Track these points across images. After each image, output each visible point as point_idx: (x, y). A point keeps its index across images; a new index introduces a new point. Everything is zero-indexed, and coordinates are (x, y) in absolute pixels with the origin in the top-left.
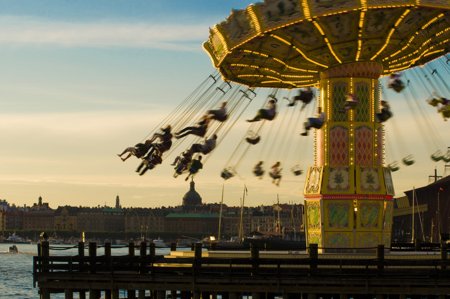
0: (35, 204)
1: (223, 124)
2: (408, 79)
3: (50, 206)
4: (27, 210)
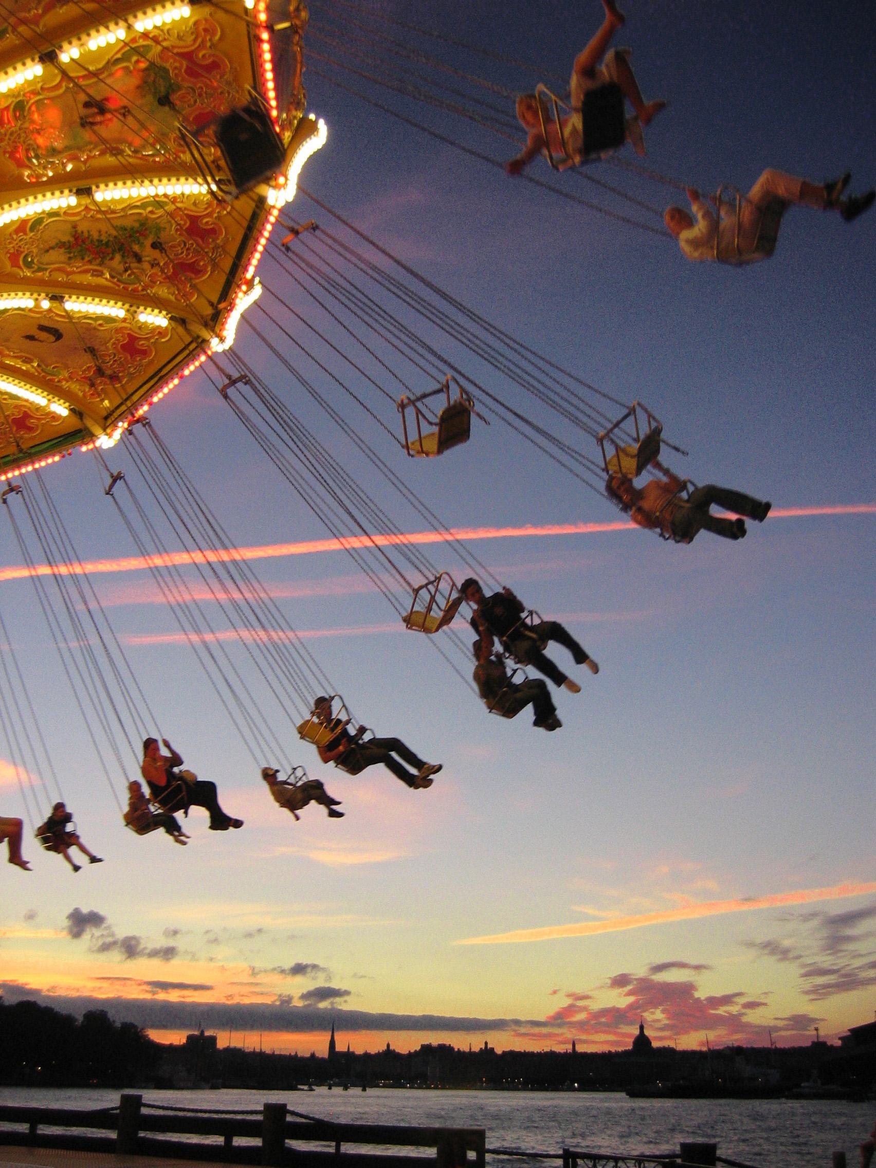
0: (481, 1049)
3: (495, 1050)
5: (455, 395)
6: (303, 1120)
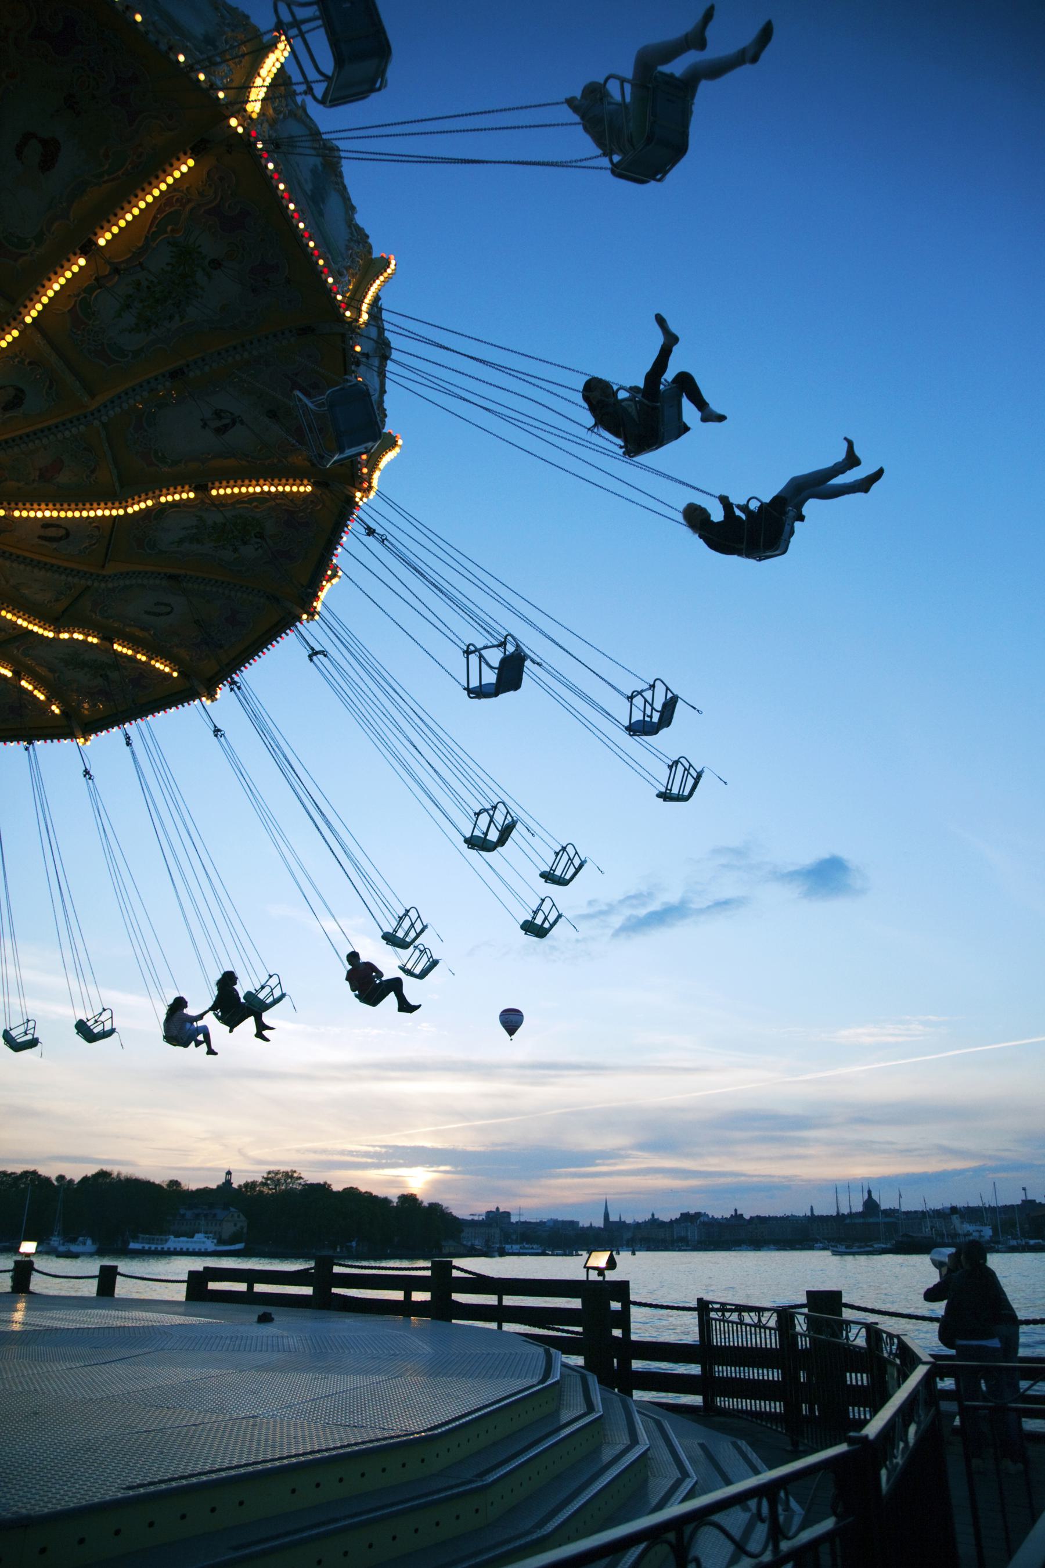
0: (732, 1215)
1: (618, 457)
2: (128, 748)
3: (744, 1216)
4: (725, 1221)
5: (511, 648)
6: (471, 1276)
